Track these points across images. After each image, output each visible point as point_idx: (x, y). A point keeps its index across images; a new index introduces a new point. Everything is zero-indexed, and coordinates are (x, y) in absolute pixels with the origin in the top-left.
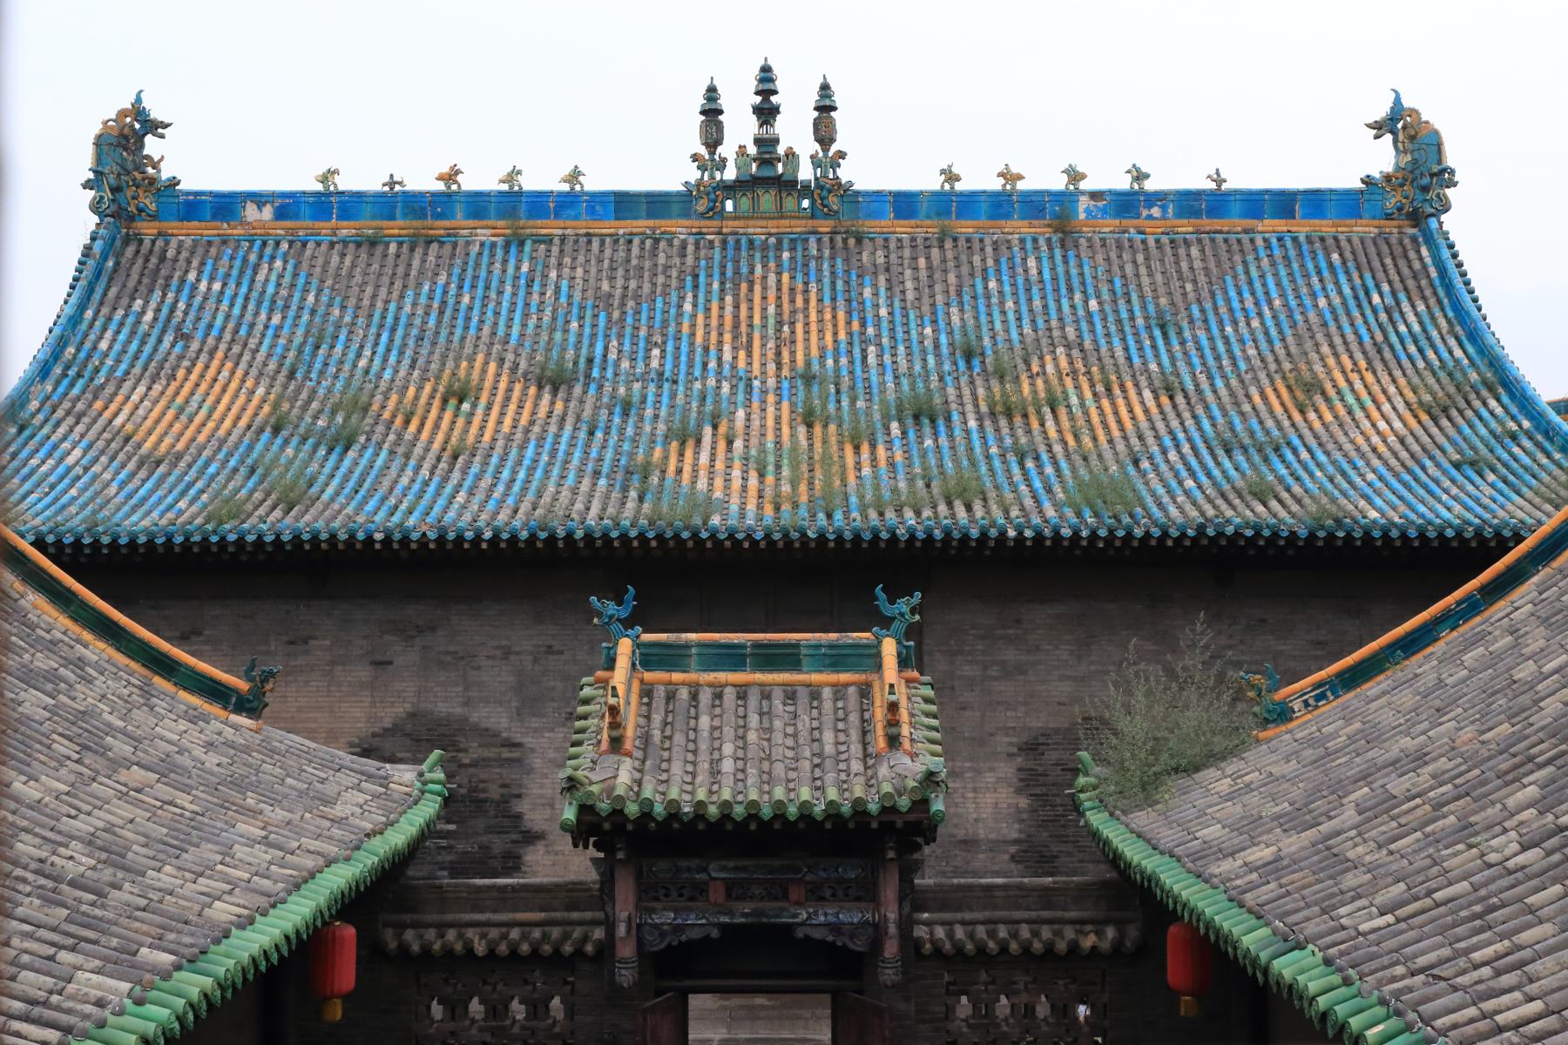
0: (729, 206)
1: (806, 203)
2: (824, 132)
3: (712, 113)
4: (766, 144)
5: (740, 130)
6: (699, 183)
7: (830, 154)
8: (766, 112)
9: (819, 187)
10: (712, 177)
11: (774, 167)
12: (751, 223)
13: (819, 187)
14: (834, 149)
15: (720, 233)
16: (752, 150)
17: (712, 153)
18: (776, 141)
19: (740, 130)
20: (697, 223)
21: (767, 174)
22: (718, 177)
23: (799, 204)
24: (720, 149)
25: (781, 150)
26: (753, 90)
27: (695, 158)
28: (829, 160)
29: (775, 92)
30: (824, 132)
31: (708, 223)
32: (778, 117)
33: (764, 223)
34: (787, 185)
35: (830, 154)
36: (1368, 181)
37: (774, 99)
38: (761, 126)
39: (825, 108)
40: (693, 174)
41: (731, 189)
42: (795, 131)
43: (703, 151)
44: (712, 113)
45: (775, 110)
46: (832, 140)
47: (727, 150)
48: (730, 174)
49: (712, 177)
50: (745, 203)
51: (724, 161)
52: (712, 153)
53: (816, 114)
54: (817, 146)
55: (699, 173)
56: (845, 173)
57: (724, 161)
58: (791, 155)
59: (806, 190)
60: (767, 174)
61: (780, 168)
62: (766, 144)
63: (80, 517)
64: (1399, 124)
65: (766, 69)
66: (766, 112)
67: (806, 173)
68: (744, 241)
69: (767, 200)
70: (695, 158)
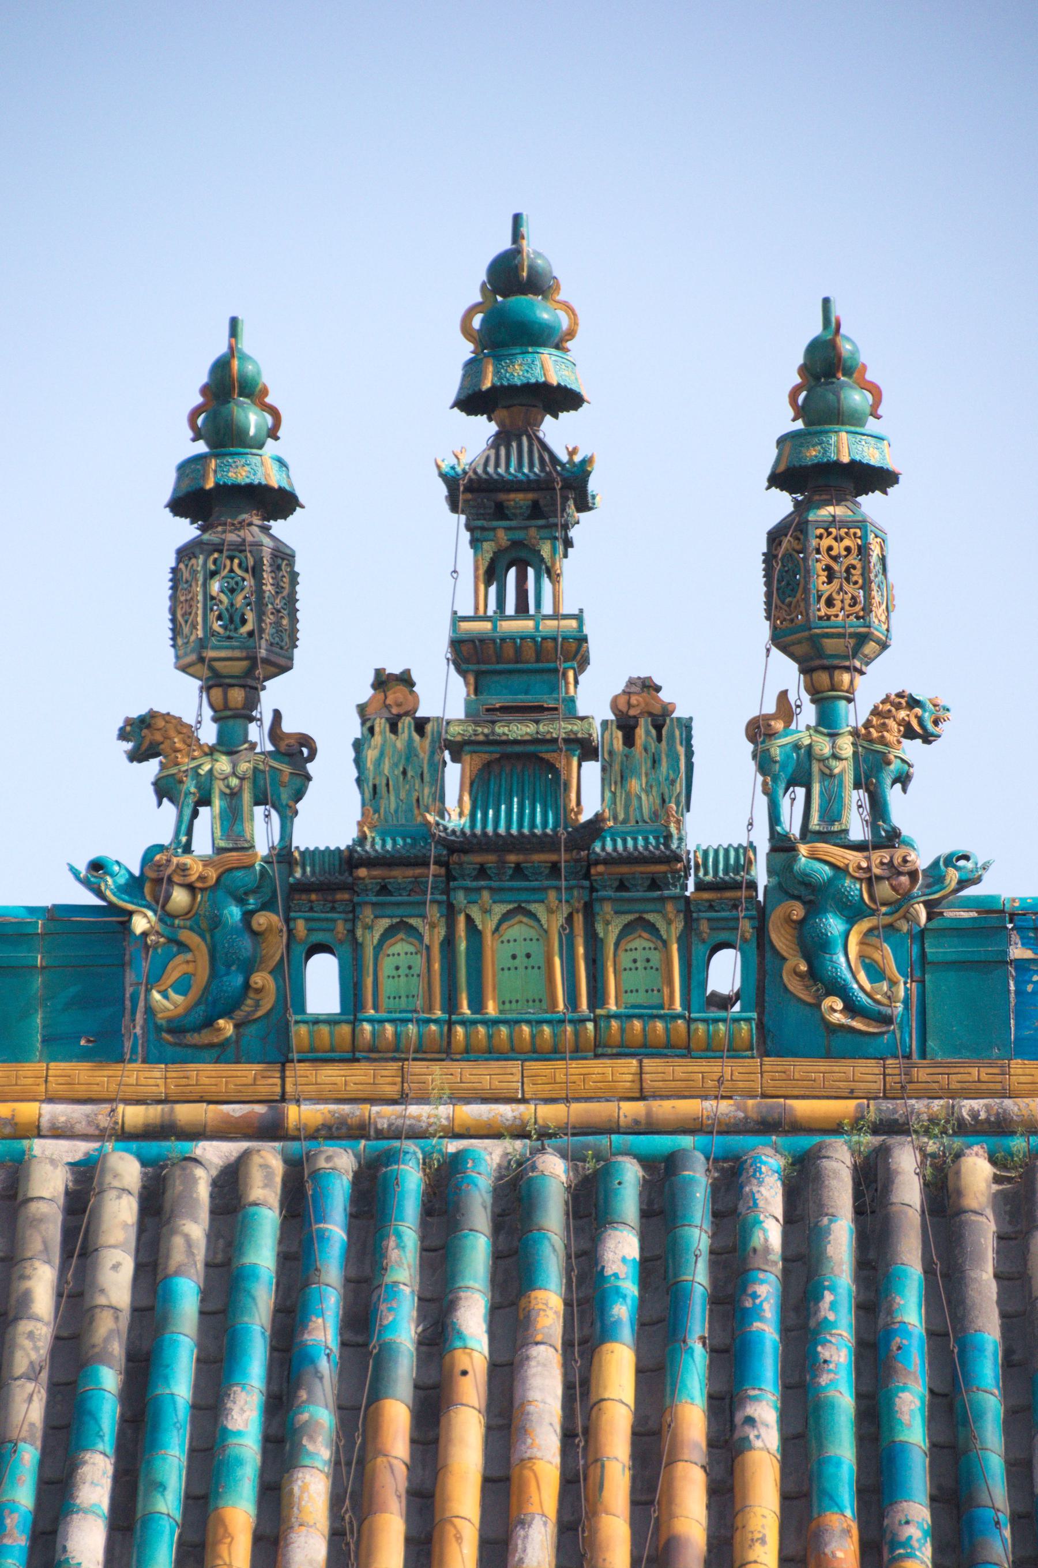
0: (322, 983)
1: (725, 972)
2: (815, 603)
3: (228, 503)
4: (516, 666)
5: (381, 593)
6: (154, 878)
7: (855, 714)
8: (520, 509)
9: (790, 882)
10: (234, 838)
11: (555, 788)
12: (435, 1074)
13: (790, 882)
14: (870, 688)
15: (271, 1130)
16: (444, 696)
17: (234, 716)
18: (572, 651)
19: (381, 593)
20: (151, 1077)
21: (520, 835)
22: (263, 831)
23: (694, 973)
24: (274, 694)
25: (594, 696)
26: (452, 385)
27: (146, 736)
28: (843, 750)
29: (564, 399)
30: (815, 603)
31: (205, 1074)
32: (585, 529)
33: (506, 1074)
34: (629, 878)
35: (855, 714)
36: (764, 576)
37: (559, 433)
38: (492, 574)
39: (820, 477)
40: (130, 820)
41: (329, 893)
42: (664, 600)
43: (184, 699)
44: (228, 503)
45: (564, 490)
46: (863, 643)
47: (316, 697)
48: (330, 817)
49: (234, 838)
50: (400, 966)
51: (296, 752)
52: (234, 716)
53: (781, 504)
54: (786, 673)
55: (160, 823)
56: (930, 817)
57: (296, 752)
58: (648, 723)
59: (721, 903)
60: (520, 835)
61: (589, 790)
62: (516, 666)
63: (142, 996)
64: (581, 611)
65: (512, 276)
66: (520, 509)
67: (724, 813)
68: (411, 1179)
69: (520, 950)
70: (146, 736)
